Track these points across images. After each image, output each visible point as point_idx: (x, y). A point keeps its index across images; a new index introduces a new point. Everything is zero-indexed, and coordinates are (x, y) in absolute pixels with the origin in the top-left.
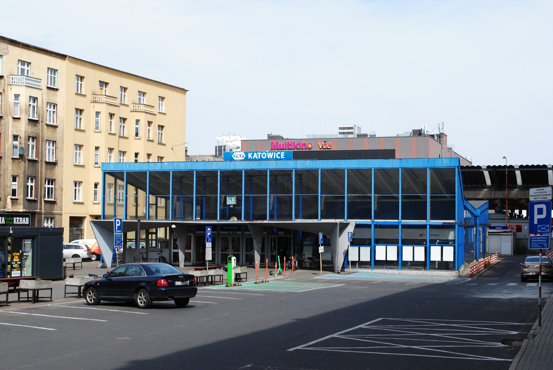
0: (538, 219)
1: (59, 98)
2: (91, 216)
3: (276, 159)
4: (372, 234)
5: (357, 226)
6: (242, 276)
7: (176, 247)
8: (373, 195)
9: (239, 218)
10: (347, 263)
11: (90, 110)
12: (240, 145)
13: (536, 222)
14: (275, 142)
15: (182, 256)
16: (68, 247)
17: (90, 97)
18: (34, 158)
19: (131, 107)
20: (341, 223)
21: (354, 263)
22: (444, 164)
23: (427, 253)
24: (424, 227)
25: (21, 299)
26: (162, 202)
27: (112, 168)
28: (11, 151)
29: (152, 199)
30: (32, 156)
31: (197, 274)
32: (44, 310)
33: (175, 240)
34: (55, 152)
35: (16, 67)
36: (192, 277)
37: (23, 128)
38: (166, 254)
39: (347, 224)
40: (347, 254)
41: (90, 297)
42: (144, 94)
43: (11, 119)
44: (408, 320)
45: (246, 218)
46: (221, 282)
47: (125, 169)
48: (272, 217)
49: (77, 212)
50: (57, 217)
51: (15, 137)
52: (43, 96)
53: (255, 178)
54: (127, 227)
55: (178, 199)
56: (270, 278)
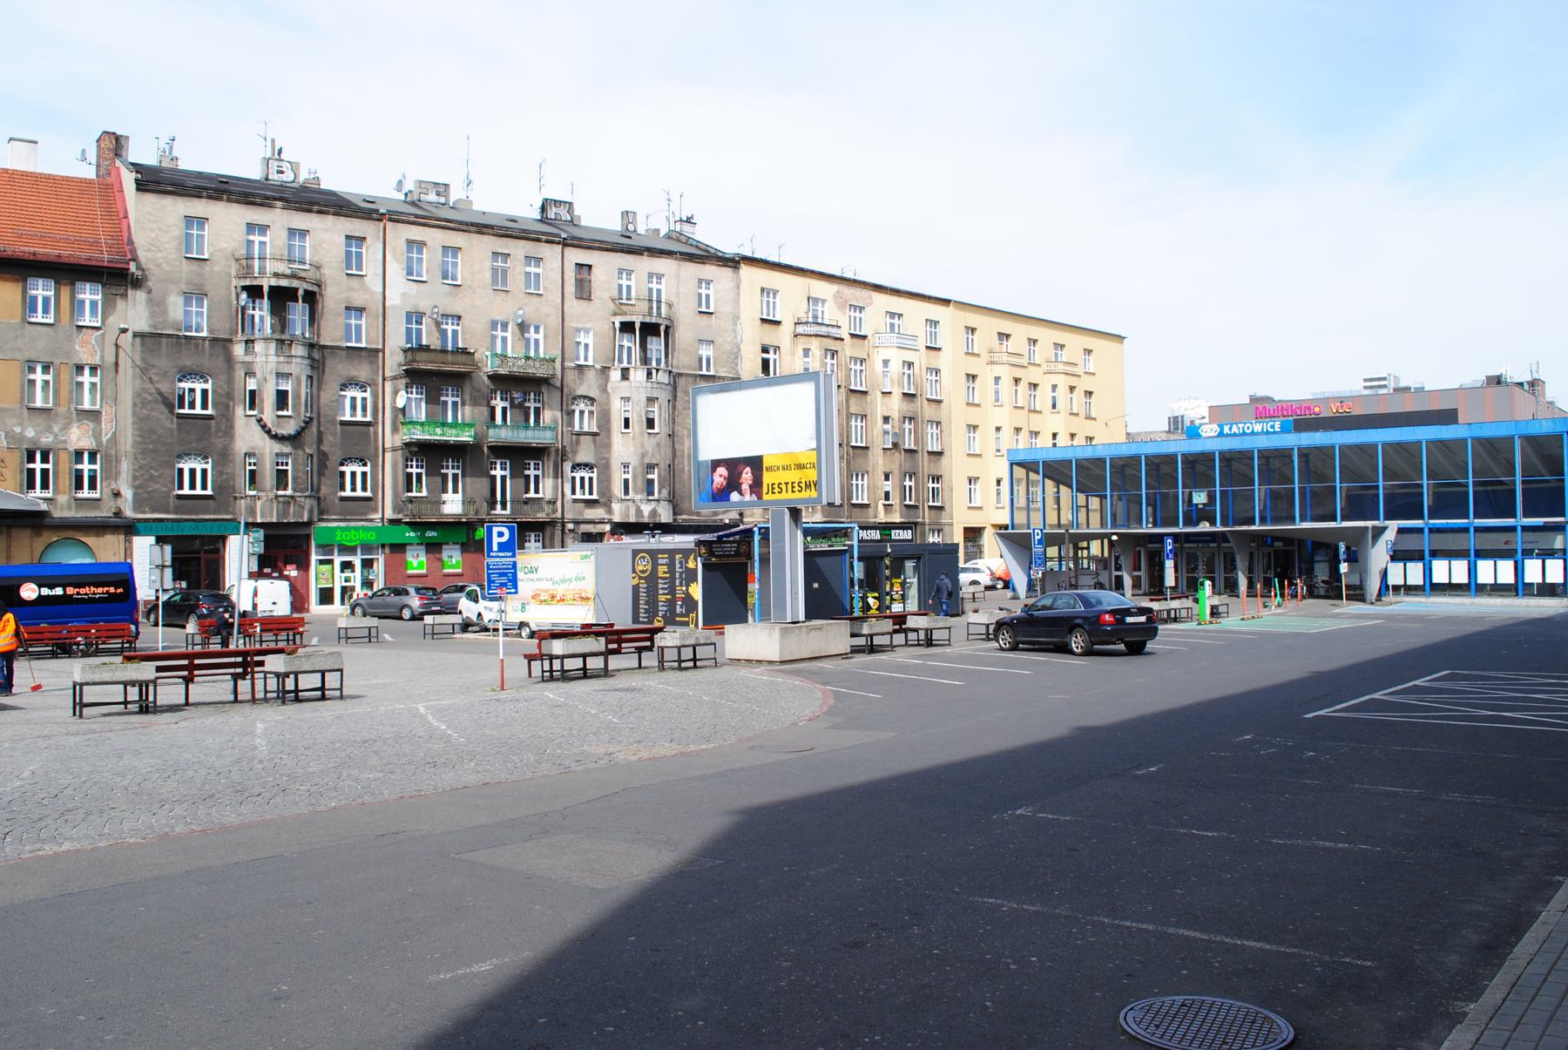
1: (943, 361)
2: (994, 526)
3: (1268, 433)
4: (1426, 543)
5: (1401, 531)
6: (1221, 609)
7: (1118, 568)
8: (1425, 482)
9: (1213, 523)
10: (1384, 587)
11: (986, 375)
12: (1206, 413)
14: (1262, 407)
15: (1128, 582)
16: (965, 570)
17: (985, 357)
18: (912, 447)
19: (1045, 367)
20: (1374, 528)
21: (1396, 588)
22: (1544, 428)
23: (1519, 571)
24: (1512, 529)
26: (1095, 503)
27: (1021, 457)
28: (880, 439)
29: (1081, 498)
30: (909, 443)
31: (1155, 606)
32: (942, 658)
33: (1117, 558)
34: (940, 438)
35: (883, 322)
36: (1150, 610)
37: (895, 406)
38: (1104, 578)
39: (1385, 529)
40: (1385, 574)
41: (1005, 639)
42: (1062, 346)
43: (879, 394)
44: (1493, 674)
45: (1224, 523)
46: (1190, 618)
47: (1041, 457)
48: (1263, 520)
49: (974, 521)
50: (946, 528)
51: (886, 419)
52: (921, 359)
53: (1236, 462)
54: (1050, 540)
55: (1120, 499)
56: (1265, 612)
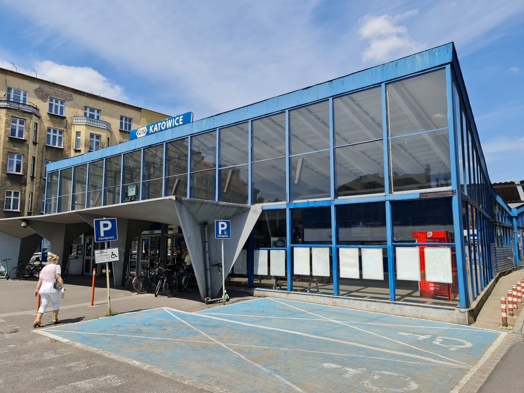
0: (104, 231)
13: (102, 234)
25: (294, 288)
41: (169, 227)
